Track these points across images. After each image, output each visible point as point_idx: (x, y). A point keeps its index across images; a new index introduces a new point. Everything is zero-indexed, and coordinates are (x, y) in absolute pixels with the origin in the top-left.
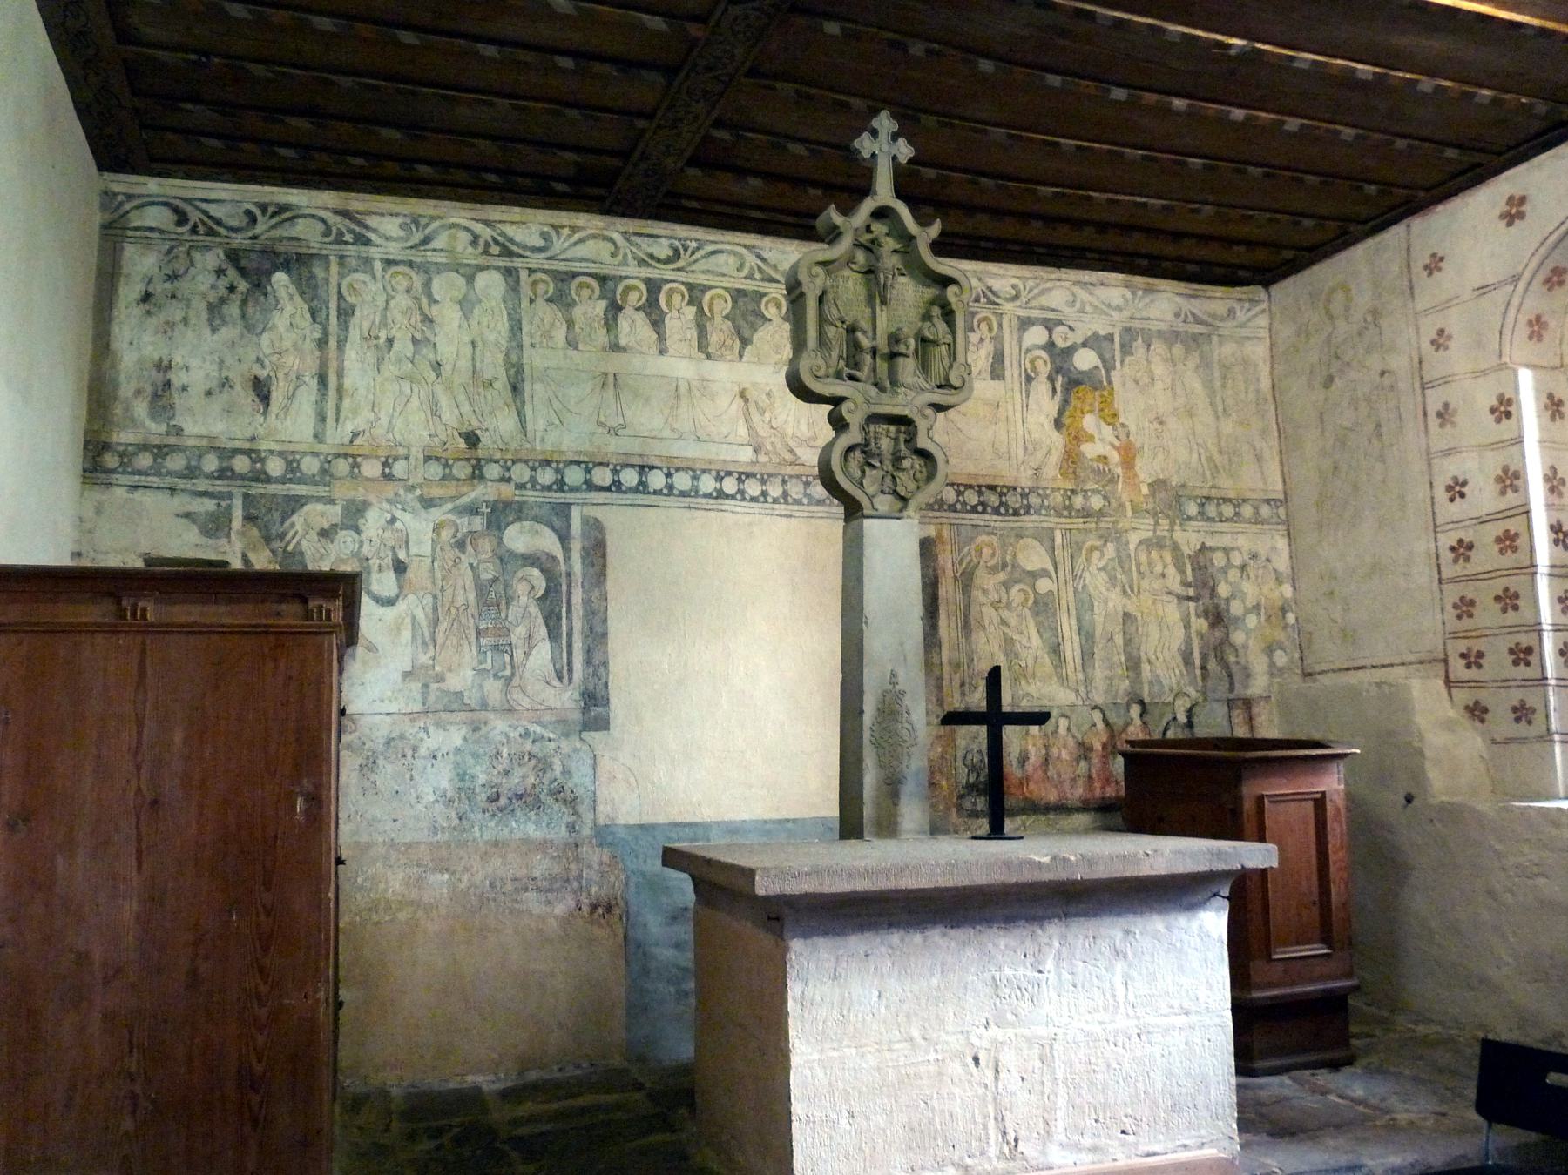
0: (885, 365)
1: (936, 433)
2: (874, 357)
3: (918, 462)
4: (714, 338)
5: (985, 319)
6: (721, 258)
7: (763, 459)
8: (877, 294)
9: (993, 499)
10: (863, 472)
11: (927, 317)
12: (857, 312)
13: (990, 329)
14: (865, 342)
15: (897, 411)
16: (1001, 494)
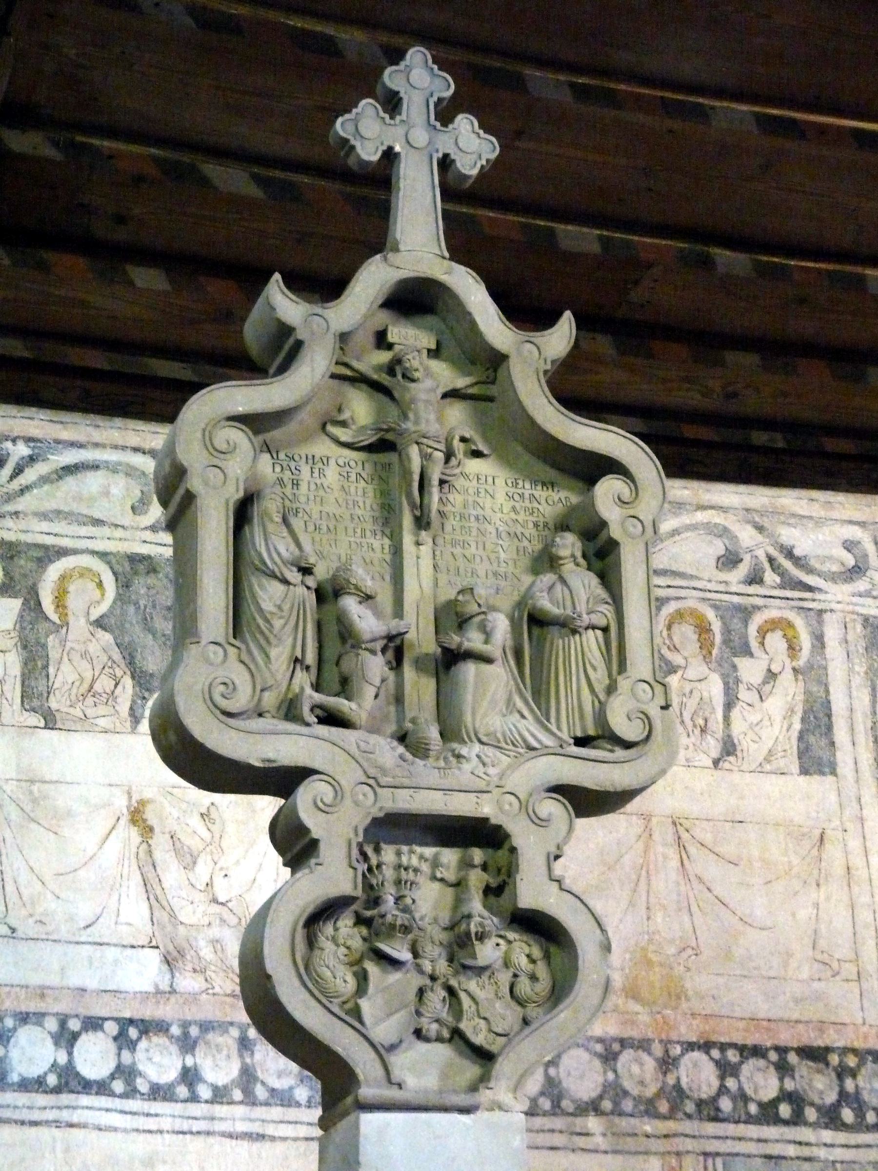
0: (429, 685)
1: (577, 868)
2: (397, 660)
3: (522, 950)
4: (65, 676)
5: (773, 625)
6: (93, 481)
7: (188, 983)
8: (405, 499)
9: (821, 1086)
10: (362, 978)
11: (546, 561)
12: (357, 552)
13: (793, 649)
14: (367, 622)
15: (462, 806)
16: (842, 1072)
